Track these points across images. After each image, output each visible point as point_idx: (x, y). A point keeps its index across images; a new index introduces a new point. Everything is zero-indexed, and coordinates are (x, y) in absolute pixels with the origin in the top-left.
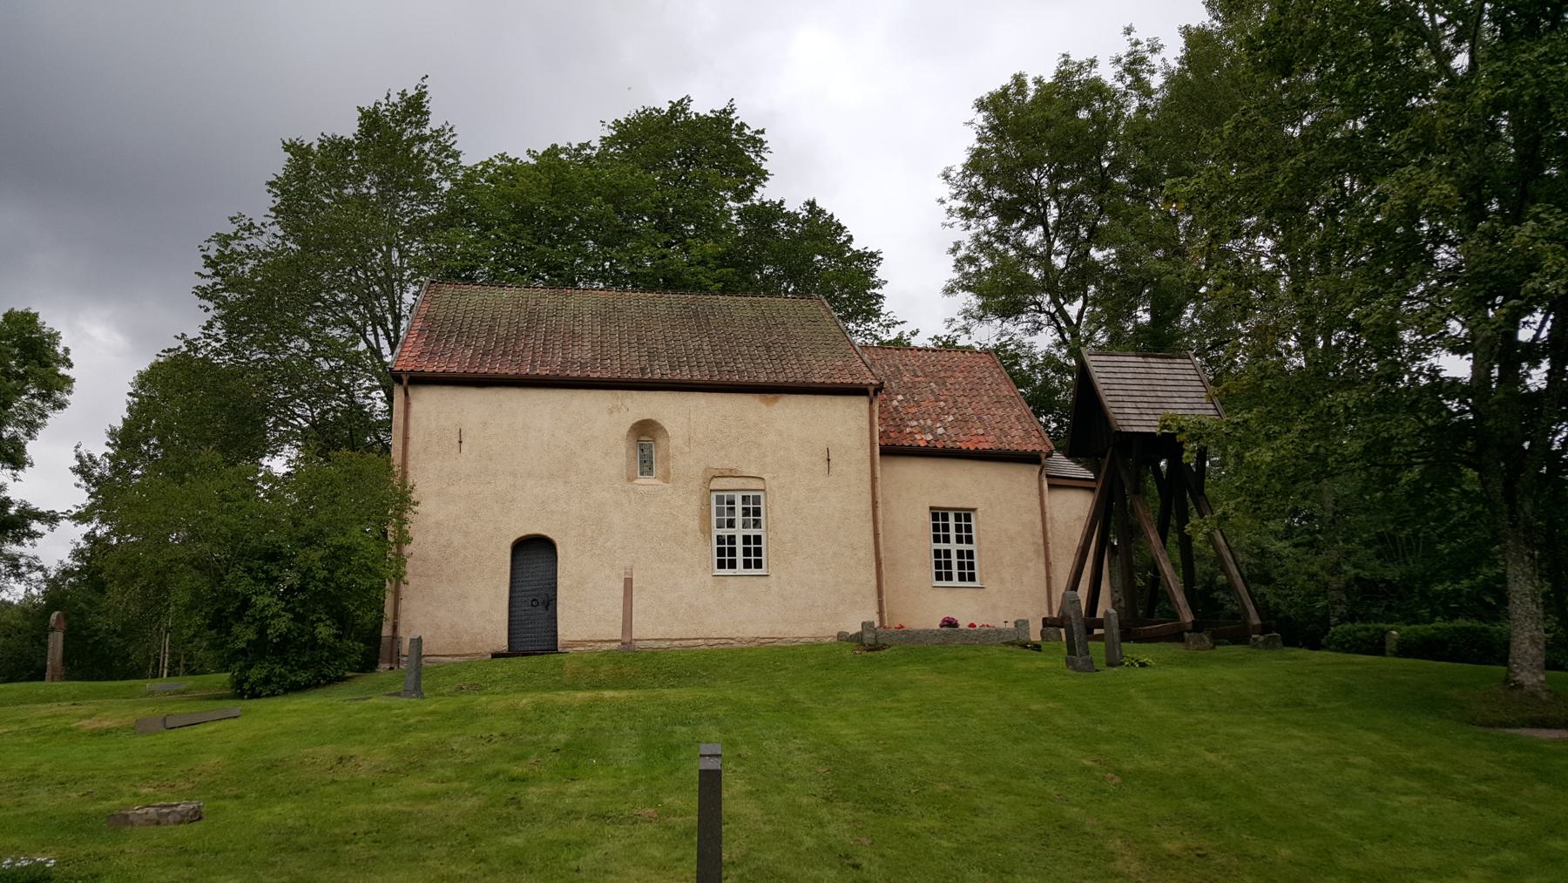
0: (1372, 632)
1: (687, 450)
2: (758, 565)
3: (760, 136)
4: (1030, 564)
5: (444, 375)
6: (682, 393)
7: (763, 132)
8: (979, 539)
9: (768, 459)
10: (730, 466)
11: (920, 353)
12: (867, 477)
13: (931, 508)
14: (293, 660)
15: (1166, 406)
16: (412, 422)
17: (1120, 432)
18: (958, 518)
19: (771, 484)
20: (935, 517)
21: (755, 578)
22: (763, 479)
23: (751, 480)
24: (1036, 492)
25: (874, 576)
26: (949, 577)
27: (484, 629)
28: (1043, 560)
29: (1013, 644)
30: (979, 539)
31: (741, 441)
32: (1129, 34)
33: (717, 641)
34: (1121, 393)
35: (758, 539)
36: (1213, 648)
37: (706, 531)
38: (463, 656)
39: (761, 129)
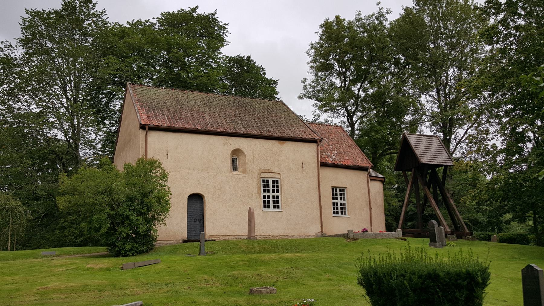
0: (485, 235)
1: (252, 161)
2: (278, 207)
3: (226, 26)
4: (365, 209)
5: (174, 128)
6: (250, 139)
7: (227, 25)
8: (348, 199)
9: (282, 166)
10: (268, 168)
11: (317, 125)
12: (316, 174)
13: (332, 187)
14: (140, 241)
15: (434, 154)
16: (148, 146)
17: (422, 163)
18: (340, 191)
19: (283, 176)
20: (333, 190)
21: (278, 212)
22: (279, 174)
23: (275, 174)
24: (366, 182)
25: (319, 212)
26: (338, 213)
27: (179, 230)
28: (369, 207)
29: (398, 238)
30: (348, 199)
31: (272, 159)
32: (379, 5)
33: (264, 236)
34: (420, 149)
35: (278, 197)
36: (457, 240)
37: (259, 194)
38: (170, 241)
39: (226, 23)
